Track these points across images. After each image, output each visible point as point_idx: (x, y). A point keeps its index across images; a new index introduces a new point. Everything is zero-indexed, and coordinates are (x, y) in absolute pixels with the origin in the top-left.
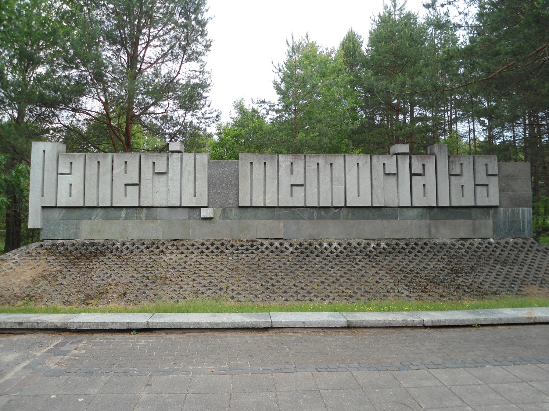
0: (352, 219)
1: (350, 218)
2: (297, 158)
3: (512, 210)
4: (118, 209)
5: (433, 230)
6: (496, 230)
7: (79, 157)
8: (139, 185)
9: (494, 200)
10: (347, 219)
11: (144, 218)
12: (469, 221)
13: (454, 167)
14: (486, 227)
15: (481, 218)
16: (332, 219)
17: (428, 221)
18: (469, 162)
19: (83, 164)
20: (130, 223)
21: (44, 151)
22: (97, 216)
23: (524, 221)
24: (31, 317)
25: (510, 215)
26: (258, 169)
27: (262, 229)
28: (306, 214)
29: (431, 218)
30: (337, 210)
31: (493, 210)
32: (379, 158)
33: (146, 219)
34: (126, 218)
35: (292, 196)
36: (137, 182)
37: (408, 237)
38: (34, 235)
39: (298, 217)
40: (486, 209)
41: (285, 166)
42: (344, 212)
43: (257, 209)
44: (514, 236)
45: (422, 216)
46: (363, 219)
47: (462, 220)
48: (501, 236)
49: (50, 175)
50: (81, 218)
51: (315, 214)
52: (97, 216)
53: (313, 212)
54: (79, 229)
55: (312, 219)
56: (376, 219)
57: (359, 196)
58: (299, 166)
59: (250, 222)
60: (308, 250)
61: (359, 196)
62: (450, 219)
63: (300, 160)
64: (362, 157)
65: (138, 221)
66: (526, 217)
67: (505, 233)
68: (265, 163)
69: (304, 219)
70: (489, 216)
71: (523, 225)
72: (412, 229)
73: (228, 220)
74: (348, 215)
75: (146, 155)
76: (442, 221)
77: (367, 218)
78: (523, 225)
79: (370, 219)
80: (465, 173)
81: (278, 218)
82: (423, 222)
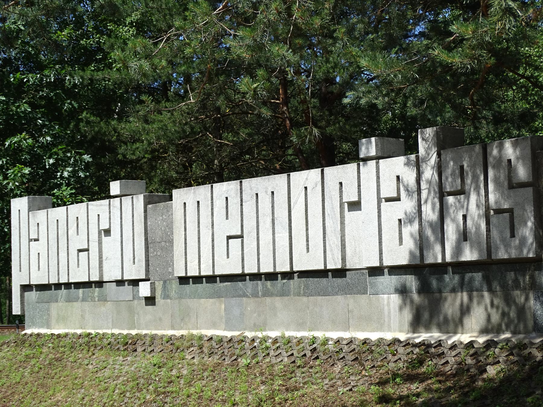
0: (304, 295)
1: (302, 292)
8: (241, 237)
10: (299, 295)
16: (281, 296)
24: (414, 338)
33: (98, 301)
34: (84, 300)
36: (239, 233)
39: (241, 293)
46: (319, 295)
49: (24, 241)
56: (337, 294)
69: (247, 296)
73: (169, 301)
74: (300, 287)
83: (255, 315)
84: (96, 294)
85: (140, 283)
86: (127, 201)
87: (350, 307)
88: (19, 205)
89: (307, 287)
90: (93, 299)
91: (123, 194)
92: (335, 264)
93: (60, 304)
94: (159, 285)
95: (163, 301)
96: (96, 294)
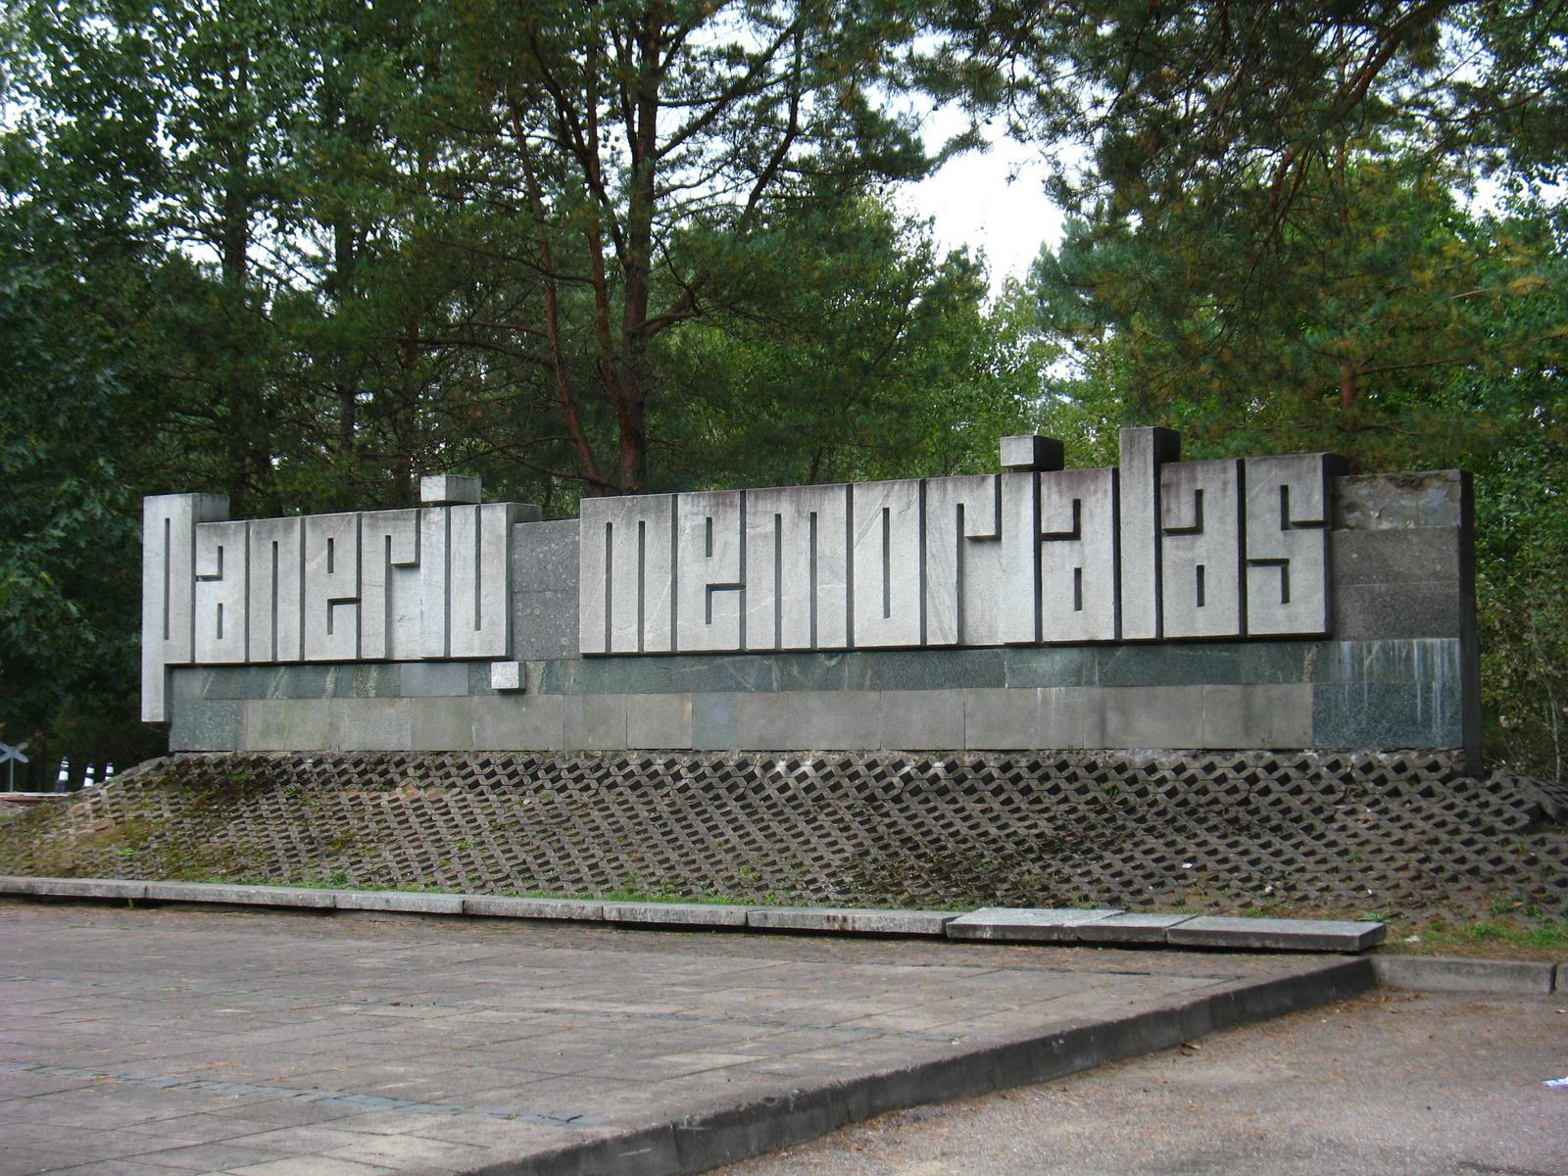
0: (872, 688)
1: (868, 683)
2: (724, 504)
3: (1383, 648)
4: (321, 669)
5: (1114, 721)
6: (1320, 722)
7: (235, 533)
8: (357, 601)
9: (1308, 617)
10: (861, 687)
11: (372, 693)
12: (1232, 688)
13: (1173, 506)
14: (1289, 712)
15: (1273, 680)
16: (821, 689)
17: (1097, 692)
18: (1225, 484)
19: (243, 548)
20: (344, 707)
21: (168, 520)
22: (277, 688)
23: (1428, 689)
25: (1376, 667)
26: (624, 543)
27: (647, 722)
28: (752, 672)
29: (1108, 681)
30: (834, 662)
31: (1314, 649)
32: (945, 490)
33: (377, 696)
34: (335, 695)
35: (709, 621)
36: (736, 580)
37: (1034, 745)
38: (156, 740)
39: (732, 683)
40: (1289, 647)
41: (693, 529)
42: (852, 666)
43: (627, 661)
44: (1390, 743)
45: (1078, 673)
46: (904, 688)
47: (1208, 687)
48: (1342, 743)
49: (180, 583)
50: (243, 696)
51: (775, 674)
52: (277, 688)
53: (770, 669)
54: (240, 723)
55: (768, 689)
56: (941, 686)
57: (887, 614)
58: (727, 535)
59: (610, 700)
60: (733, 784)
61: (887, 614)
62: (1170, 683)
63: (729, 510)
64: (897, 487)
65: (361, 701)
66: (1437, 671)
67: (1360, 733)
68: (642, 525)
69: (745, 689)
70: (1300, 670)
71: (1426, 701)
72: (1046, 717)
73: (561, 697)
74: (863, 676)
75: (372, 517)
76: (1143, 690)
77: (918, 684)
78: (1426, 701)
79: (925, 688)
80: (1208, 523)
81: (678, 688)
82: (1080, 695)
83: (763, 722)
84: (371, 684)
85: (493, 664)
86: (463, 516)
87: (969, 708)
88: (165, 516)
89: (878, 674)
90: (362, 694)
91: (451, 499)
92: (945, 637)
93: (273, 703)
94: (537, 671)
95: (544, 698)
96: (371, 684)
